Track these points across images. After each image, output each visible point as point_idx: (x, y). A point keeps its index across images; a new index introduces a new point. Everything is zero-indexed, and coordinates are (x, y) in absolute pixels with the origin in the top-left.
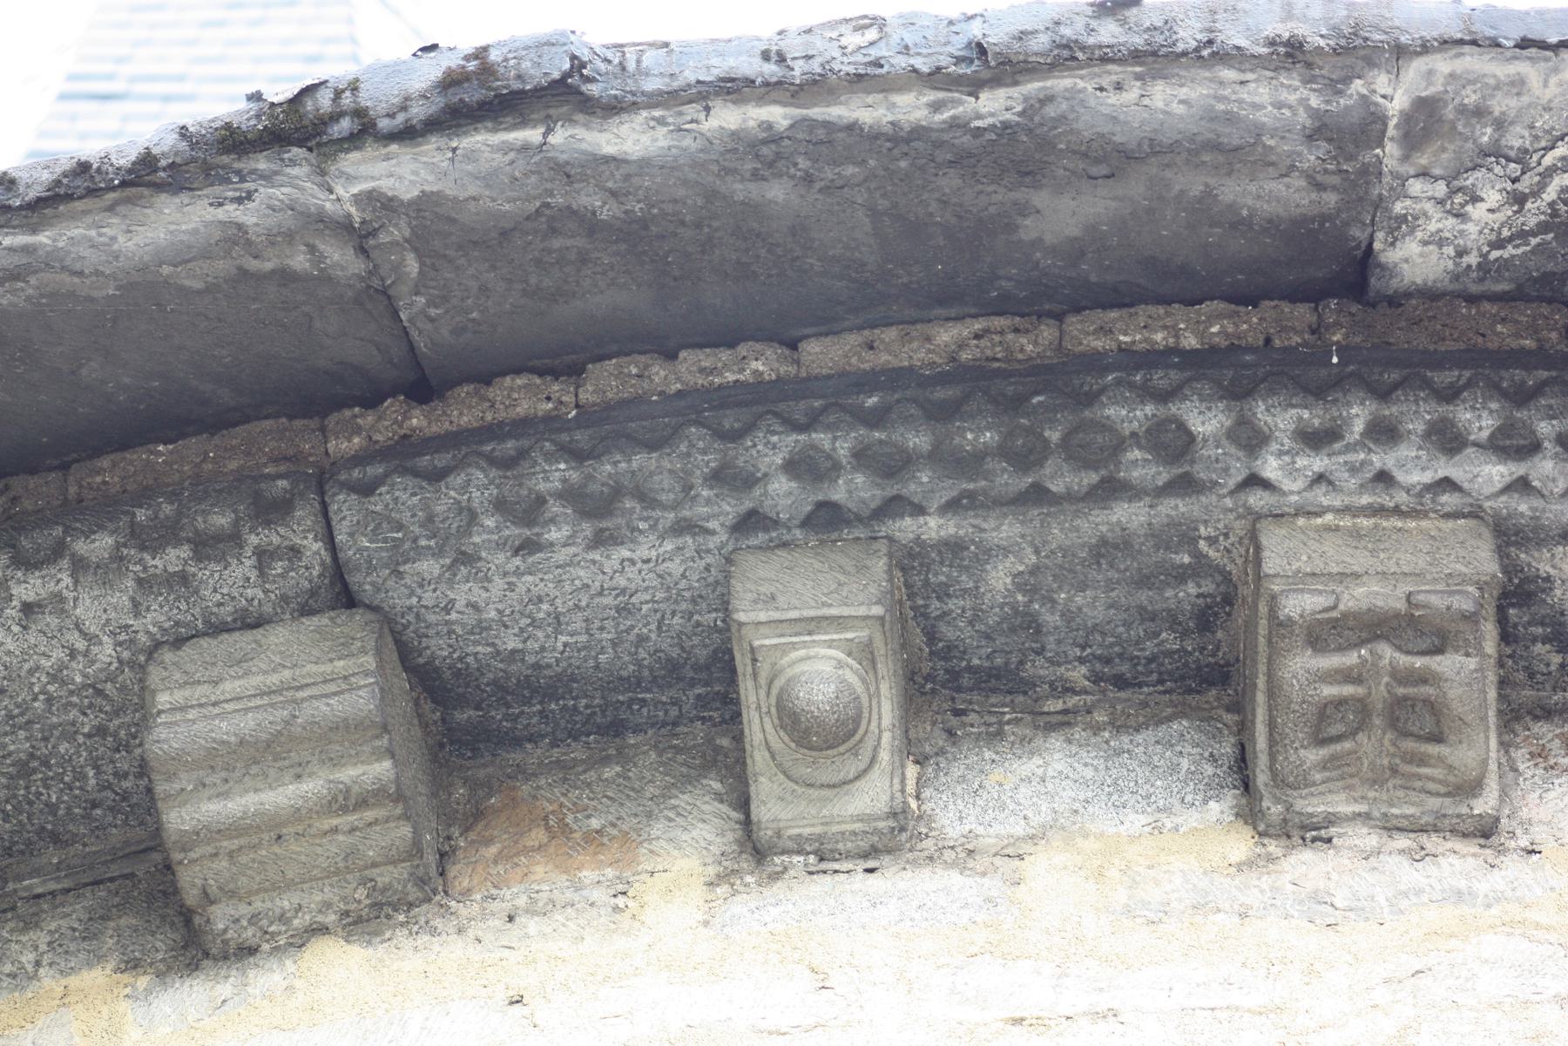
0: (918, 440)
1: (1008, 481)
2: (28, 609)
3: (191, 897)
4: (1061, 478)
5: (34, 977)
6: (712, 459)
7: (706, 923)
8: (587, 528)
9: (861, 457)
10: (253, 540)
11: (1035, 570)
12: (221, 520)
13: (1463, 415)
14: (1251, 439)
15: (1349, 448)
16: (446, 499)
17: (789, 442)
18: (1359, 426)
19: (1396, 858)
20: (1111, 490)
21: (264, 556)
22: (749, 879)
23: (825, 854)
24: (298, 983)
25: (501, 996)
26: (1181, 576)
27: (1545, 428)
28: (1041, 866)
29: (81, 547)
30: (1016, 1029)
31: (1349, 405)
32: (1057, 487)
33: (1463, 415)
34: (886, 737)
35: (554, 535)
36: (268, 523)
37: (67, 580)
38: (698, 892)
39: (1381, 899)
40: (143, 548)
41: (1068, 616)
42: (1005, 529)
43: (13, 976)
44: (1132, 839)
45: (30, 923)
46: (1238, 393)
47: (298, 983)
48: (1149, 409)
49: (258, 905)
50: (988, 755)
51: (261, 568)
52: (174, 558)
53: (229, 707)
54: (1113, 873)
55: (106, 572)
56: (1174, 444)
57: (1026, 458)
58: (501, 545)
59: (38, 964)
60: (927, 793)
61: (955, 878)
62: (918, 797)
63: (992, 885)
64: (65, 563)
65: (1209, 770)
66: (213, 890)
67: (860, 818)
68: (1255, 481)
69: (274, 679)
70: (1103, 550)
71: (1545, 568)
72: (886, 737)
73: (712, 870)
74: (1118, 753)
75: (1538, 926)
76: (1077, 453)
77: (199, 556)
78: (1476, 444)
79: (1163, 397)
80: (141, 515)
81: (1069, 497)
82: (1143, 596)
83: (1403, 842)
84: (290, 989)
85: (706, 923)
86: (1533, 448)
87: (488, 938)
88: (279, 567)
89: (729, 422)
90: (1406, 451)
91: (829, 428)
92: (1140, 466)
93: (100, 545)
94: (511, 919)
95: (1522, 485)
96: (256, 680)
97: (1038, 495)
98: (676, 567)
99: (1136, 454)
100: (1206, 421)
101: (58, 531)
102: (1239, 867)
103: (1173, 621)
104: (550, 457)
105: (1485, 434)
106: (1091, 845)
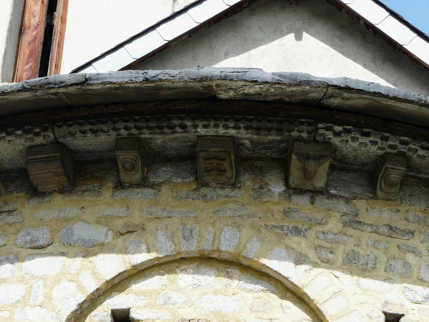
0: (144, 125)
1: (158, 131)
2: (9, 141)
3: (35, 186)
4: (166, 130)
5: (13, 192)
6: (112, 126)
7: (112, 196)
8: (94, 135)
9: (136, 127)
10: (42, 134)
11: (164, 141)
12: (37, 130)
13: (229, 123)
14: (196, 127)
15: (211, 128)
16: (72, 129)
17: (124, 124)
18: (212, 125)
19: (218, 189)
20: (174, 132)
21: (44, 136)
22: (119, 188)
23: (132, 186)
24: (51, 200)
25: (81, 207)
26: (187, 142)
27: (242, 125)
28: (164, 189)
29: (17, 132)
30: (156, 219)
31: (211, 121)
32: (165, 131)
33: (229, 123)
34: (140, 168)
35: (88, 135)
36: (44, 131)
37: (14, 137)
38: (111, 190)
39: (215, 197)
40: (26, 134)
41: (171, 146)
42: (159, 136)
43: (9, 191)
44: (179, 183)
45: (13, 182)
46: (193, 119)
47: (51, 200)
48: (180, 121)
49: (45, 187)
50: (158, 166)
51: (44, 138)
52: (31, 136)
53: (39, 160)
54: (175, 190)
55: (20, 136)
56: (183, 127)
57: (160, 128)
58: (80, 136)
59: (14, 190)
60: (148, 173)
61: (150, 190)
62: (147, 174)
63: (155, 191)
64: (14, 135)
65: (192, 170)
66: (38, 185)
67: (136, 179)
68: (196, 131)
69: (46, 156)
70: (174, 139)
71: (244, 142)
72: (140, 168)
73: (114, 186)
74: (178, 166)
75: (238, 202)
76: (169, 127)
77: (34, 136)
78: (231, 127)
79: (182, 119)
80: (26, 127)
81: (168, 133)
82: (182, 144)
83: (220, 186)
84: (50, 201)
85: (112, 196)
86: (239, 128)
87: (80, 195)
88: (47, 137)
89: (115, 119)
90: (220, 128)
91: (130, 122)
92: (178, 129)
93: (20, 132)
94: (83, 192)
95: (239, 133)
96: (43, 156)
97: (163, 133)
98: (108, 140)
99: (178, 128)
100: (189, 123)
101: (13, 129)
102: (194, 190)
103: (187, 147)
104: (88, 124)
105: (232, 126)
106: (172, 184)
